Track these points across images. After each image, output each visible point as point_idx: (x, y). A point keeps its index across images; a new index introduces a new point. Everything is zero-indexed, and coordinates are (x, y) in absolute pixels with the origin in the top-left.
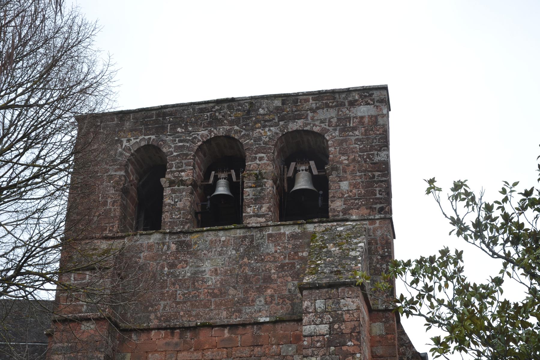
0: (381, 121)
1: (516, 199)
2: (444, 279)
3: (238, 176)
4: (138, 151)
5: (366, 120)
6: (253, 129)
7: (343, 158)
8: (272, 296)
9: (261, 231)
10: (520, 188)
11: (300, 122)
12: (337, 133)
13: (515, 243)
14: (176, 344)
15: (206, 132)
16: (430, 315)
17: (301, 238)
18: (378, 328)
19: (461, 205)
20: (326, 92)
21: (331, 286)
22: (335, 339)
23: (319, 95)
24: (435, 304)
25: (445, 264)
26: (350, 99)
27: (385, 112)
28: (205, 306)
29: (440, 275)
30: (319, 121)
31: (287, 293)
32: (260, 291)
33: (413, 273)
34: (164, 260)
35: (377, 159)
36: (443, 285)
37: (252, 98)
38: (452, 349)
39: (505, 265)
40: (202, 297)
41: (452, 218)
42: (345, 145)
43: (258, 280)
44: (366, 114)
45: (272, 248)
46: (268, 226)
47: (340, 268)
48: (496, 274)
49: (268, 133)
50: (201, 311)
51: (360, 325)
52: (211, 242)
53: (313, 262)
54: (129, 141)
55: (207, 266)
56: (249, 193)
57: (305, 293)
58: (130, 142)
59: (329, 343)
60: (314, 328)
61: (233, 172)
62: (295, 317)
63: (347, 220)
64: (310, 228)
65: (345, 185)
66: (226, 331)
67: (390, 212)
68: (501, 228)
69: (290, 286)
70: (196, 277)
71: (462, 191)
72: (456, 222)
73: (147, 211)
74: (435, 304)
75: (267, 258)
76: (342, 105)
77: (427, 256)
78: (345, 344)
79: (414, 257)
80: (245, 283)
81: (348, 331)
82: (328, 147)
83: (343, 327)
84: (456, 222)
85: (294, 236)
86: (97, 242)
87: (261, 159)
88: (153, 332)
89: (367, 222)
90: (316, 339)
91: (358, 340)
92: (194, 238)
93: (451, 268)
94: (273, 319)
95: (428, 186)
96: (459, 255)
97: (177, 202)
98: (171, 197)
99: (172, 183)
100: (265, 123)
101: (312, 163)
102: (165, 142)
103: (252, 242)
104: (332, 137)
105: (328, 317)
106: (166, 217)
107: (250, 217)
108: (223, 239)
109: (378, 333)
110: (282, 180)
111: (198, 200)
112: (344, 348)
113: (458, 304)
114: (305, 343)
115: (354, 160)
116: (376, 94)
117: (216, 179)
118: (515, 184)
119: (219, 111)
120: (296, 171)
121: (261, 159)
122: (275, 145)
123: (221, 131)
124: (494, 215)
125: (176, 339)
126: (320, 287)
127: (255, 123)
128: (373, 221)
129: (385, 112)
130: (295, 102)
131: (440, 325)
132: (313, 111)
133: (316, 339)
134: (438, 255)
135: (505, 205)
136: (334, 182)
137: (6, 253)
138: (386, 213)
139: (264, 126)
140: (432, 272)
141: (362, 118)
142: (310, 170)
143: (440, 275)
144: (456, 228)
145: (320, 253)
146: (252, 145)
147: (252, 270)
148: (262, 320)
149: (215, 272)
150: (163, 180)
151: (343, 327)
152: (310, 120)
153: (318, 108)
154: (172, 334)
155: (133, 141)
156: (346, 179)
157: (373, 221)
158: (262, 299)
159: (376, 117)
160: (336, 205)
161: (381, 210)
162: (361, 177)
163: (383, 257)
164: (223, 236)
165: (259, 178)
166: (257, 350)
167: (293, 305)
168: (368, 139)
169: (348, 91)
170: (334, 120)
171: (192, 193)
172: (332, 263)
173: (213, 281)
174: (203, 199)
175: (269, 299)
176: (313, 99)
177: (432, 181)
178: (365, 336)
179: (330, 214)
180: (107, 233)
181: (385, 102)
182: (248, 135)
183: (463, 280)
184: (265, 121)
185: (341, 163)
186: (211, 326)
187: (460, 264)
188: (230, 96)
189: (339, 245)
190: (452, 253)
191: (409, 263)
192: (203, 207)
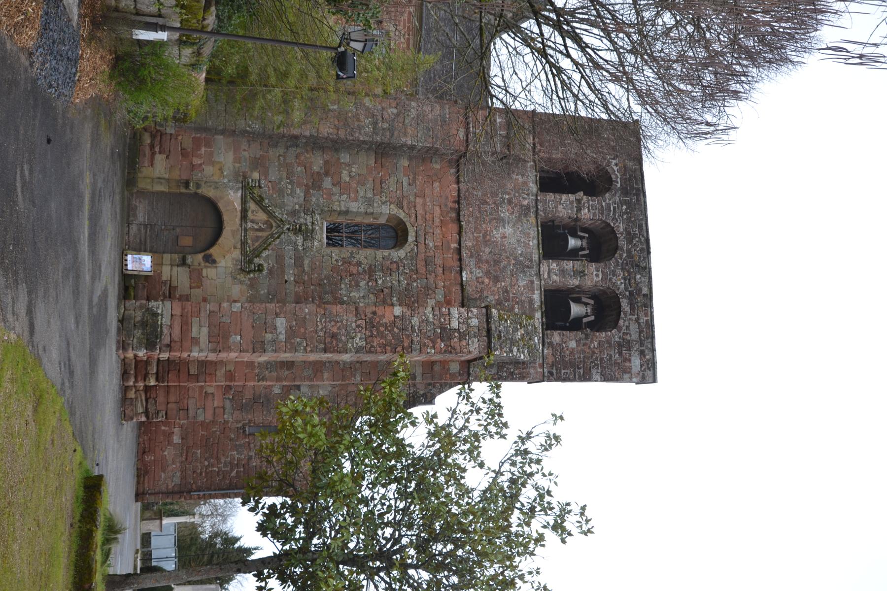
0: (626, 376)
1: (544, 483)
2: (485, 423)
3: (583, 256)
4: (607, 172)
5: (627, 364)
6: (623, 269)
7: (596, 344)
8: (483, 283)
9: (536, 275)
10: (553, 488)
11: (627, 309)
12: (617, 340)
13: (513, 481)
14: (446, 205)
15: (621, 229)
16: (458, 412)
17: (530, 307)
18: (455, 368)
19: (542, 440)
20: (653, 332)
21: (489, 331)
22: (446, 334)
23: (650, 326)
24: (466, 416)
25: (496, 424)
26: (646, 352)
27: (634, 380)
28: (476, 228)
29: (489, 421)
30: (628, 323)
31: (485, 295)
32: (488, 273)
33: (491, 400)
34: (515, 196)
35: (594, 371)
36: (481, 422)
37: (650, 269)
38: (428, 427)
39: (494, 471)
40: (484, 226)
41: (531, 433)
42: (606, 345)
43: (497, 272)
44: (632, 364)
45: (522, 283)
46: (541, 280)
47: (503, 339)
48: (487, 464)
49: (619, 282)
50: (472, 225)
51: (457, 353)
52: (529, 234)
53: (509, 317)
54: (616, 165)
55: (509, 230)
56: (569, 265)
57: (484, 310)
58: (614, 168)
59: (443, 329)
60: (456, 316)
61: (587, 252)
62: (466, 301)
63: (543, 345)
64: (538, 315)
65: (573, 344)
66: (456, 245)
67: (549, 380)
68: (523, 471)
69: (491, 298)
70: (501, 221)
71: (553, 442)
72: (529, 436)
73: (553, 182)
74: (466, 416)
75: (514, 279)
76: (642, 345)
77: (503, 411)
78: (442, 340)
79: (503, 401)
80: (495, 261)
81: (452, 344)
82: (606, 331)
83: (456, 340)
84: (529, 436)
85: (531, 301)
86: (530, 140)
87: (597, 276)
88: (456, 186)
89: (541, 361)
90: (447, 318)
91: (445, 352)
92: (532, 219)
93: (493, 429)
94: (464, 283)
95: (558, 415)
96: (503, 437)
97: (563, 206)
98: (567, 200)
99: (579, 201)
100: (628, 280)
101: (592, 318)
102: (614, 195)
103: (528, 267)
104: (614, 335)
105: (463, 328)
106: (550, 196)
107: (549, 266)
108: (531, 243)
109: (451, 368)
110: (579, 292)
111: (564, 222)
112: (439, 340)
113: (466, 433)
114: (444, 309)
115: (594, 353)
116: (649, 373)
117: (582, 238)
118: (556, 483)
119: (640, 241)
120: (586, 304)
121: (597, 276)
122: (608, 288)
123: (622, 242)
124: (532, 465)
125: (450, 205)
126: (488, 323)
127: (628, 271)
128: (542, 366)
129: (634, 380)
130: (645, 305)
131: (450, 419)
132: (637, 320)
133: (447, 318)
134: (504, 421)
135: (540, 474)
136: (576, 335)
137: (516, 74)
138: (548, 377)
139: (625, 279)
140: (492, 414)
141: (630, 361)
142: (587, 316)
143: (489, 421)
144: (524, 435)
145: (516, 323)
146: (609, 268)
147: (505, 267)
148: (464, 274)
149: (504, 237)
150: (581, 194)
151: (456, 340)
152: (629, 317)
153: (639, 324)
154: (455, 202)
155: (616, 168)
156: (577, 346)
157: (542, 366)
158: (481, 274)
159: (630, 372)
160: (556, 337)
161: (551, 373)
162: (579, 358)
163: (512, 374)
164: (533, 243)
165: (582, 274)
166: (440, 270)
167: (476, 299)
168: (611, 365)
169: (653, 350)
170: (628, 337)
171: (570, 217)
172: (508, 332)
173: (497, 235)
174: (565, 227)
175: (480, 280)
176: (647, 321)
177: (561, 418)
178: (448, 357)
179: (549, 332)
180: (538, 147)
181: (643, 380)
182: (618, 265)
183: (484, 438)
184: (629, 280)
185: (592, 342)
186: (460, 233)
187: (496, 437)
188: (652, 250)
189: (522, 338)
190: (504, 431)
191: (498, 396)
192: (558, 227)
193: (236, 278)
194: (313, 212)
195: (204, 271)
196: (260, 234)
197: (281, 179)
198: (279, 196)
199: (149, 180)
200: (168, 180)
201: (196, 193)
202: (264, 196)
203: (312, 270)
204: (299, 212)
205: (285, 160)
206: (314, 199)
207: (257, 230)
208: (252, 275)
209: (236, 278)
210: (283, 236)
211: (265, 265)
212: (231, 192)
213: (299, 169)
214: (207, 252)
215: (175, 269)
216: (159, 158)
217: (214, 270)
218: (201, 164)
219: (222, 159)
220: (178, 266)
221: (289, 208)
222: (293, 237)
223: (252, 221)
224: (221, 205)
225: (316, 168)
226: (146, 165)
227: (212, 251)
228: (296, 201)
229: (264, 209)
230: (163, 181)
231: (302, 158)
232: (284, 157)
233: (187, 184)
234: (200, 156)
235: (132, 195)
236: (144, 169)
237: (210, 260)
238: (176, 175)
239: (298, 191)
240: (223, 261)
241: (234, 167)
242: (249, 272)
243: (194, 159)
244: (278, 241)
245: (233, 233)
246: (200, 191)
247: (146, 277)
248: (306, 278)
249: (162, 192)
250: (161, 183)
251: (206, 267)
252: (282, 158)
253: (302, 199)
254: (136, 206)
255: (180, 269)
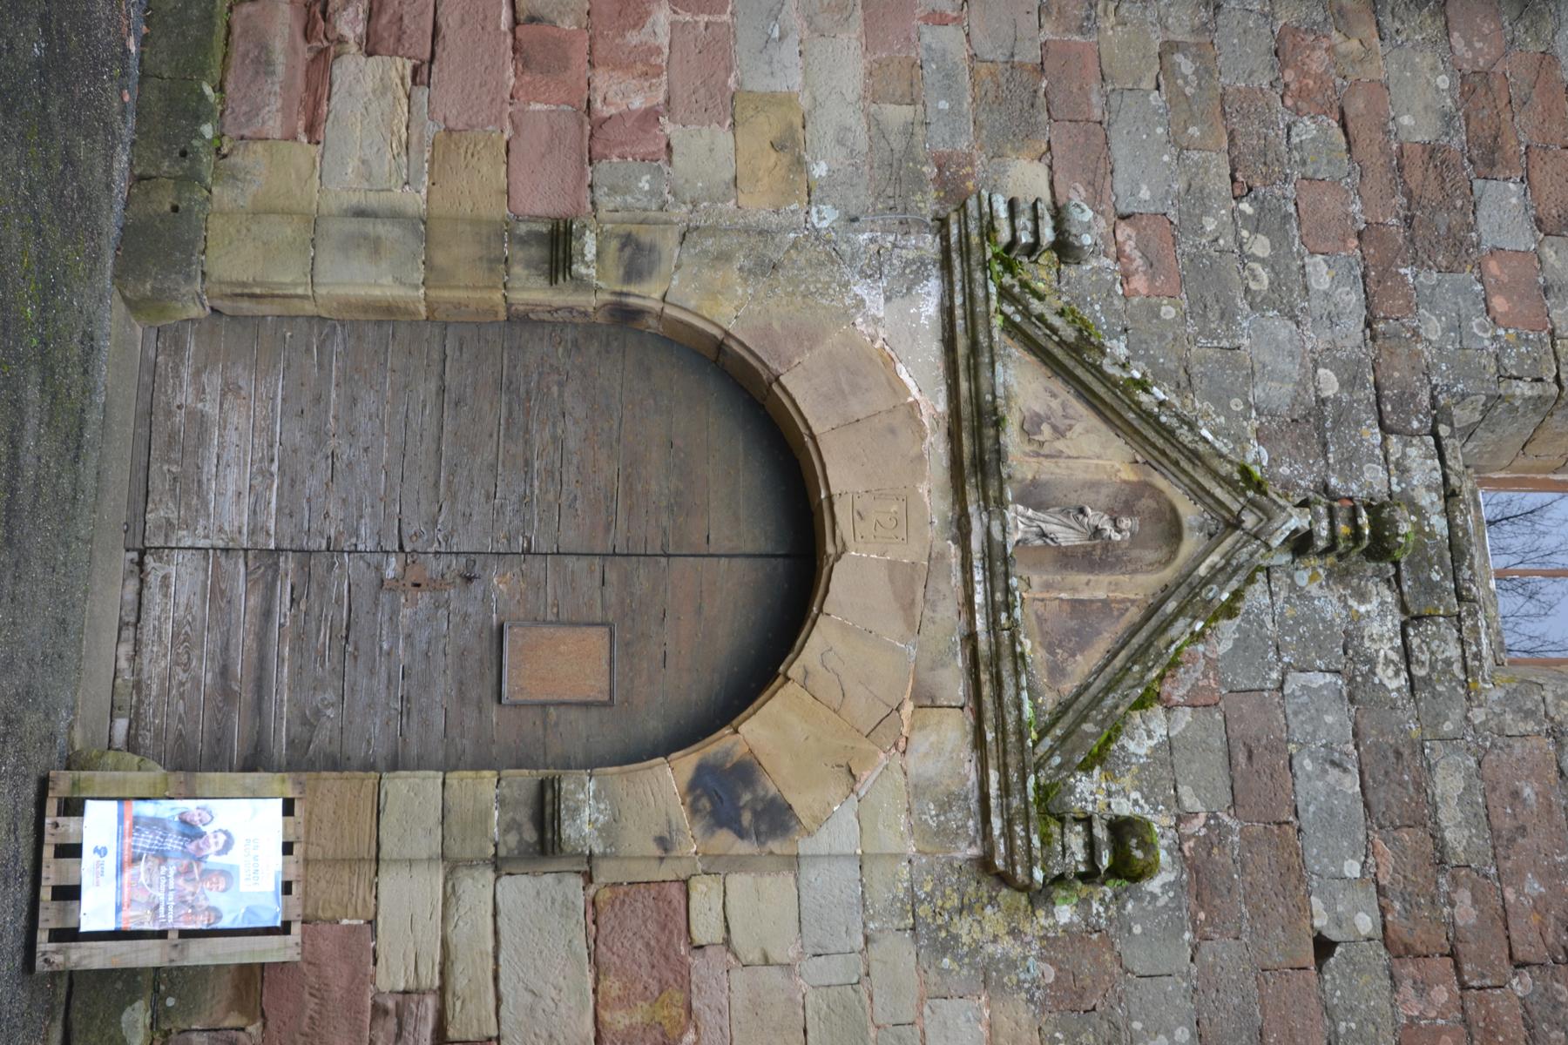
193: (947, 946)
194: (1438, 414)
195: (705, 895)
196: (1097, 587)
197: (1196, 198)
198: (1198, 308)
199: (288, 231)
200: (424, 228)
201: (625, 315)
202: (1094, 311)
203: (1500, 842)
204: (1343, 416)
205: (1206, 72)
206: (1433, 328)
207: (1067, 559)
208: (1065, 913)
209: (947, 946)
210: (1257, 595)
211: (1161, 822)
212: (871, 295)
213: (1307, 130)
214: (722, 744)
215: (477, 887)
216: (365, 84)
217: (777, 888)
218: (650, 117)
219: (791, 79)
220: (499, 865)
221: (1276, 392)
222: (1329, 603)
223: (1034, 495)
224: (804, 390)
225: (1415, 124)
226: (273, 125)
227: (761, 732)
228: (1316, 340)
229: (1113, 404)
230: (382, 229)
231: (1318, 61)
232: (1204, 55)
233: (557, 250)
234: (644, 64)
235: (172, 338)
236: (252, 159)
237: (741, 807)
238: (479, 188)
239: (1320, 274)
240: (845, 813)
241: (875, 125)
242: (1040, 897)
243: (604, 81)
244: (1228, 632)
245: (908, 586)
246: (647, 295)
247: (250, 978)
248: (1465, 912)
249: (387, 315)
250: (375, 247)
251: (718, 866)
252: (1186, 66)
253: (1353, 326)
254: (199, 422)
255: (517, 889)
